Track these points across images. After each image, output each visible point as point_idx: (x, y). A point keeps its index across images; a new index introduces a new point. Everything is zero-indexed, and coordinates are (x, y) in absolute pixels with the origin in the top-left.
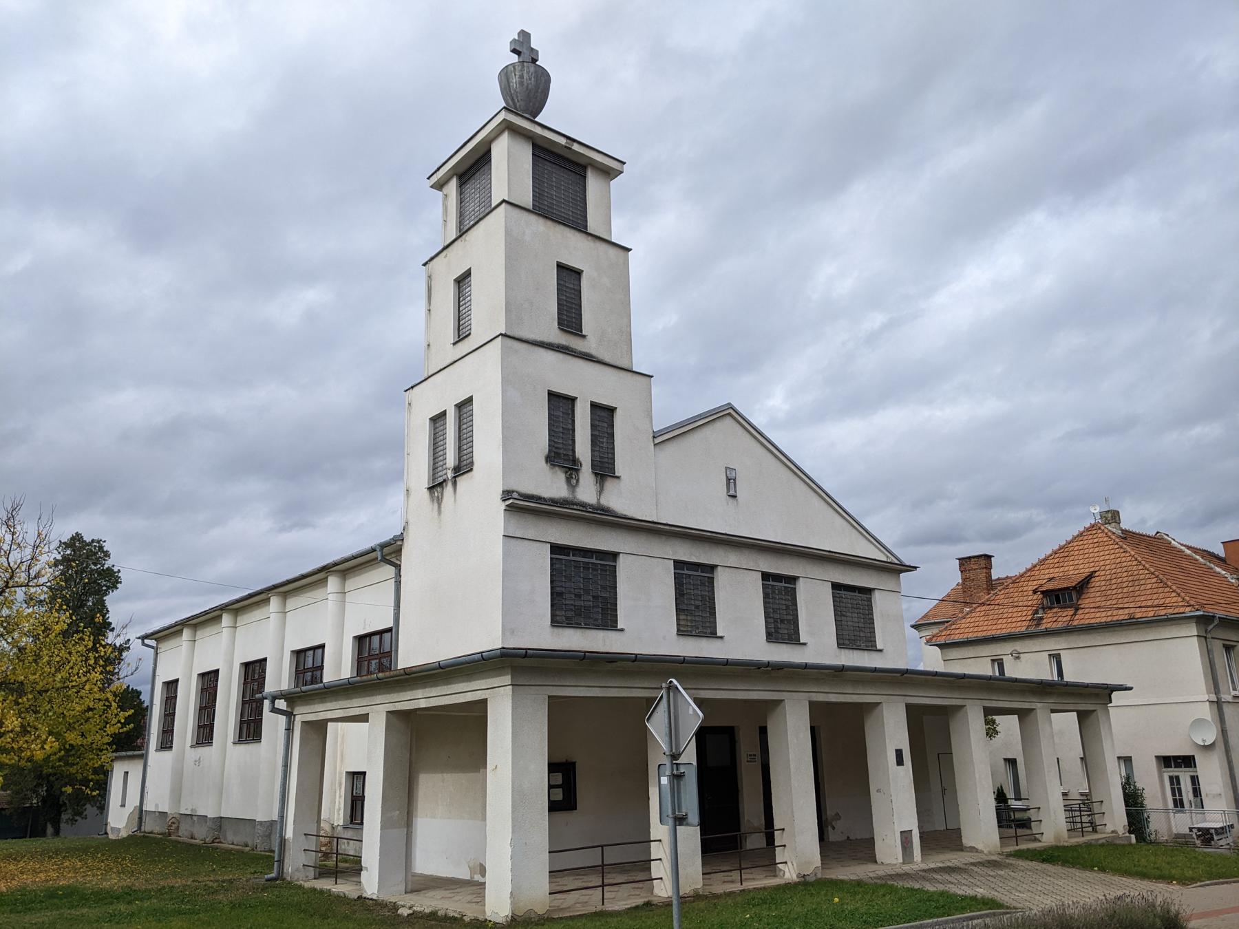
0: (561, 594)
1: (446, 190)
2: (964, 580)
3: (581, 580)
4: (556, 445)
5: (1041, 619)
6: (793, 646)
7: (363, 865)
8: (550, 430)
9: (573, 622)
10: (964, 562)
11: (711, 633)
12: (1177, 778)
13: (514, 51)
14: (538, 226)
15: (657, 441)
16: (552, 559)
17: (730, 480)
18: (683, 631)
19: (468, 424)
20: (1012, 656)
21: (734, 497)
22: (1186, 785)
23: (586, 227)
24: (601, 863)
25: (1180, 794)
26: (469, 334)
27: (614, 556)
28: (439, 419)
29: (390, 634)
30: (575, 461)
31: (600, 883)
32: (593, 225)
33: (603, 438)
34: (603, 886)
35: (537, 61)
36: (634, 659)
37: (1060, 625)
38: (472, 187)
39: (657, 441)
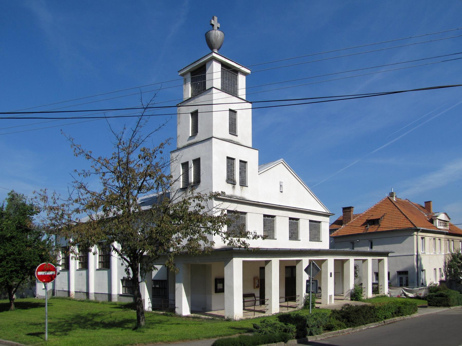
1: (185, 77)
2: (344, 215)
5: (368, 229)
7: (176, 306)
10: (344, 209)
12: (402, 278)
14: (224, 95)
21: (282, 192)
22: (404, 280)
25: (402, 282)
33: (242, 173)
37: (373, 231)
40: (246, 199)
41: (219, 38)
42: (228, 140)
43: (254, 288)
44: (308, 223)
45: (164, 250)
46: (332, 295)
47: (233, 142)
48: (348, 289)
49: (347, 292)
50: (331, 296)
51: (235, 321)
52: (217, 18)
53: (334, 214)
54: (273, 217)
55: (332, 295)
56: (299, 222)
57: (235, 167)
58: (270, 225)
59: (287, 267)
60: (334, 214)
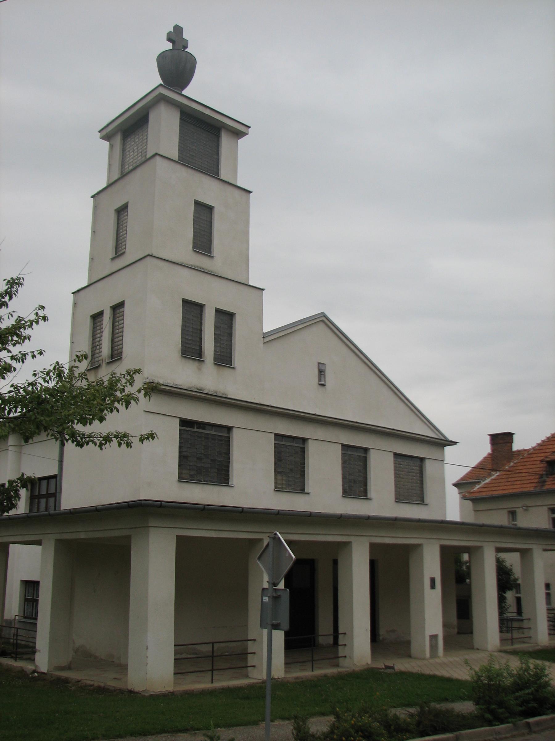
0: (186, 457)
2: (493, 450)
6: (362, 500)
8: (183, 330)
9: (195, 479)
11: (301, 489)
13: (169, 40)
14: (183, 173)
15: (267, 339)
16: (180, 430)
19: (120, 318)
20: (522, 508)
21: (323, 385)
26: (124, 252)
27: (229, 429)
28: (97, 317)
29: (54, 480)
31: (210, 668)
32: (224, 175)
34: (212, 670)
35: (186, 47)
36: (241, 510)
38: (133, 143)
39: (267, 339)
40: (229, 396)
44: (390, 460)
45: (538, 669)
50: (434, 638)
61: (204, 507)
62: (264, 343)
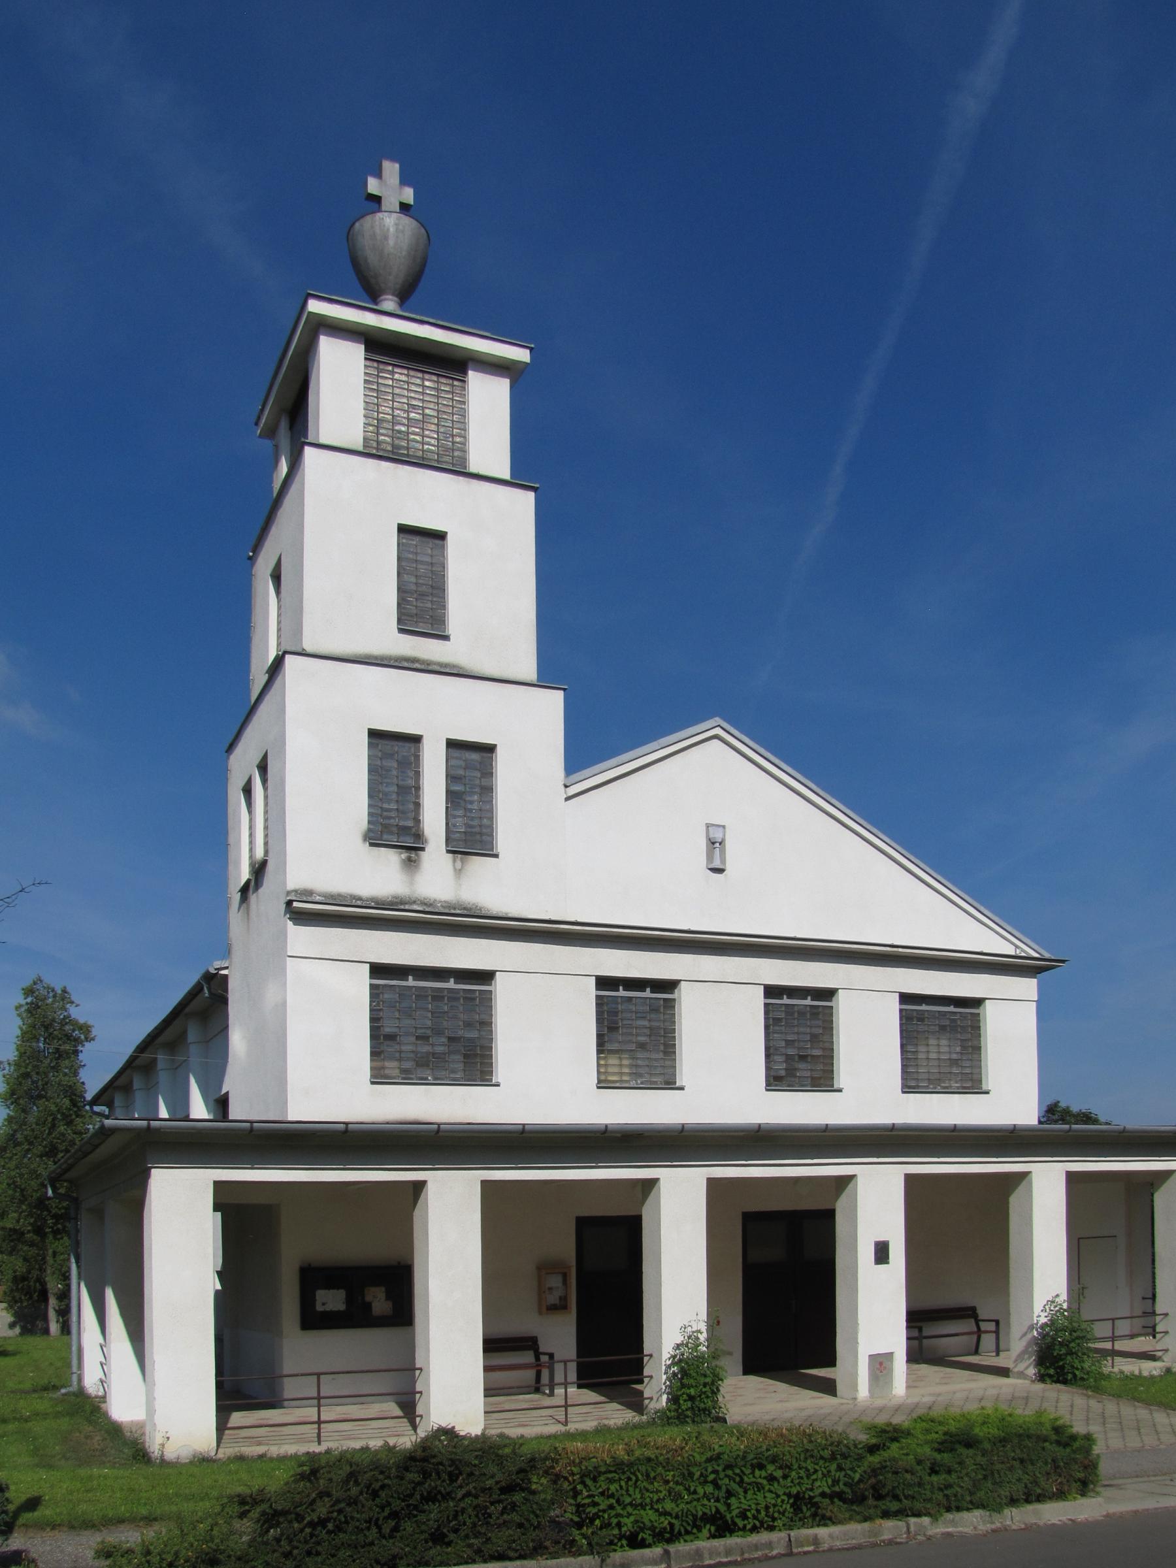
3: (429, 1015)
4: (385, 814)
17: (713, 843)
18: (910, 1087)
21: (720, 871)
23: (464, 461)
24: (569, 1408)
30: (419, 836)
40: (483, 913)
41: (391, 242)
42: (390, 658)
43: (540, 1313)
46: (890, 1356)
47: (422, 667)
48: (1027, 1324)
49: (1025, 1335)
50: (881, 1363)
51: (164, 1463)
52: (397, 166)
53: (1063, 961)
54: (669, 986)
55: (890, 1356)
56: (675, 996)
57: (423, 771)
58: (646, 1023)
59: (749, 1219)
60: (1063, 961)
61: (347, 1128)
62: (568, 799)
